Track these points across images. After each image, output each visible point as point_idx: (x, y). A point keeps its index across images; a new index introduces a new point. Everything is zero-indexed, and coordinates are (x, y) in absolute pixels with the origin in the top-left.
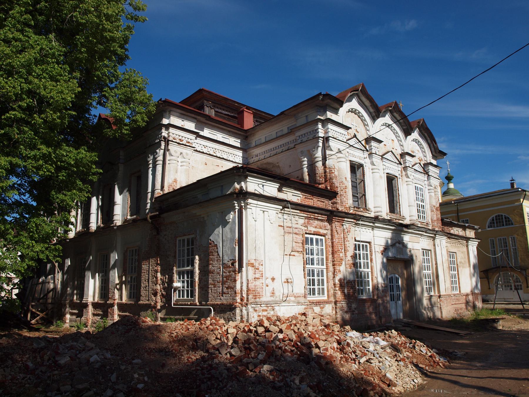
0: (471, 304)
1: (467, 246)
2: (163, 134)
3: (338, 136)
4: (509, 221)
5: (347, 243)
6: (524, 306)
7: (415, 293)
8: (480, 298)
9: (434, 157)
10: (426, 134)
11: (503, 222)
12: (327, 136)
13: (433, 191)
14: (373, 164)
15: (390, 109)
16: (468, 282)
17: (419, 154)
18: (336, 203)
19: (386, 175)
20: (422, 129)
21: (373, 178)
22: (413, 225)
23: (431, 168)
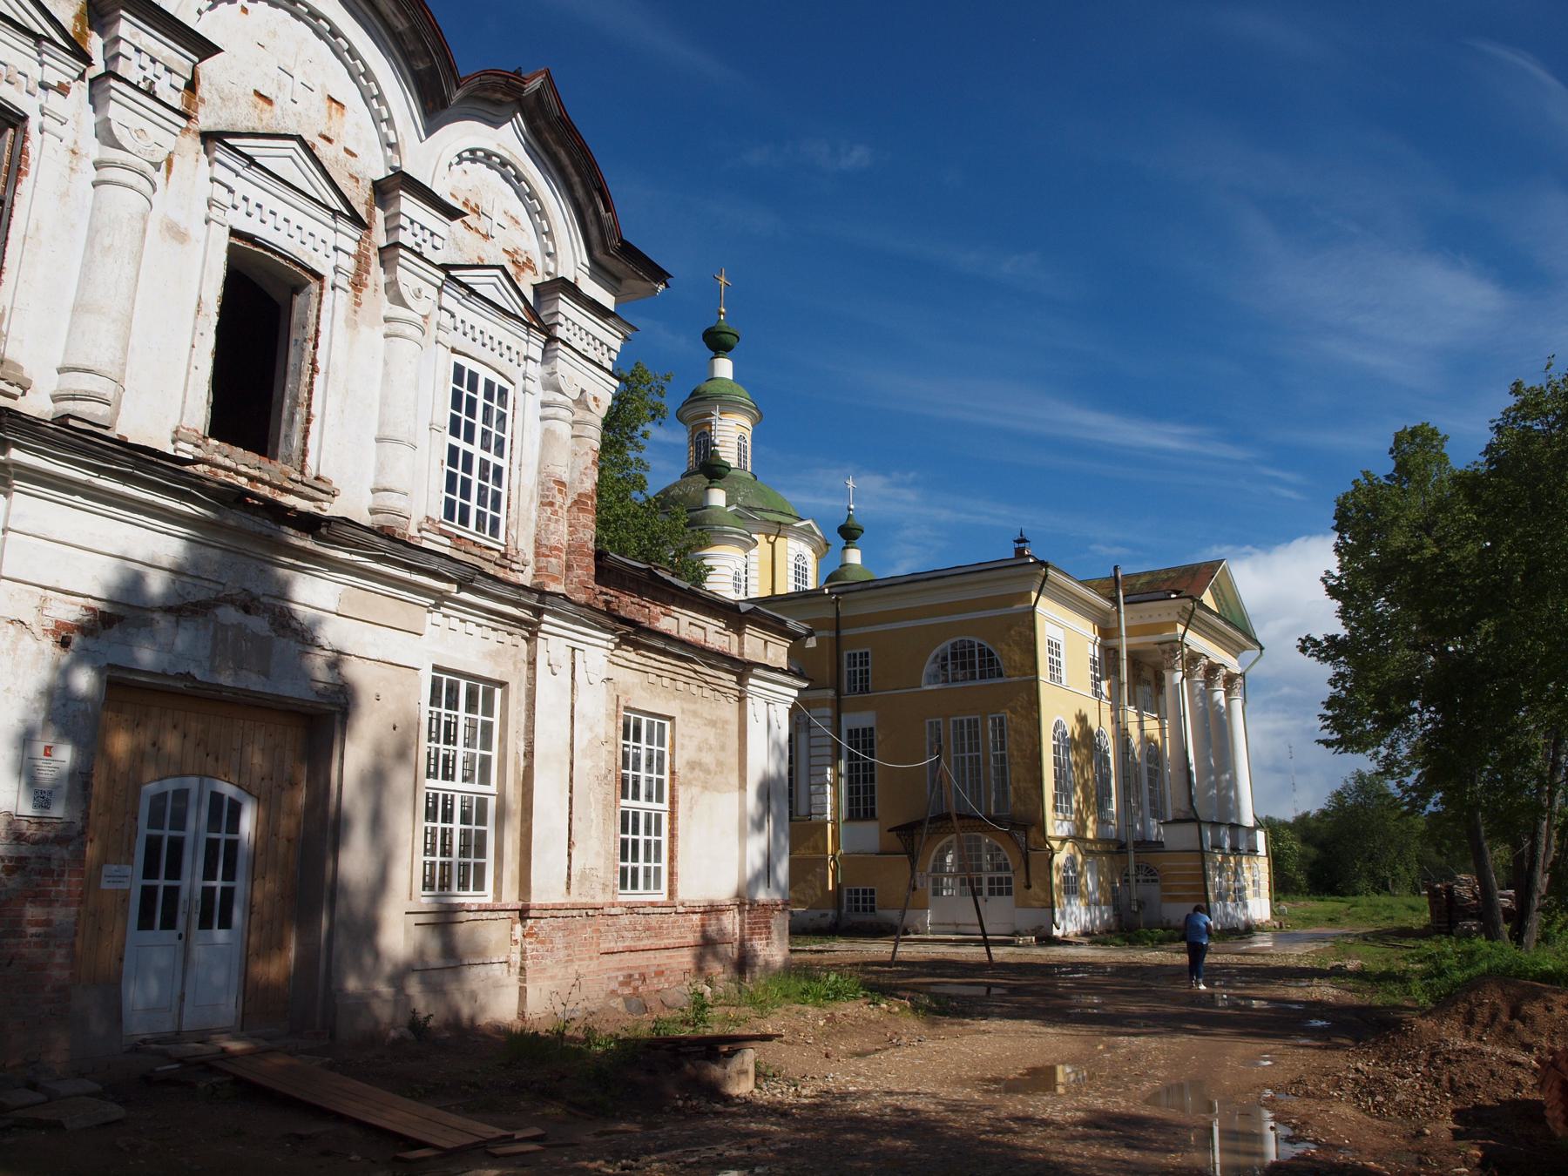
0: (732, 951)
1: (741, 699)
6: (993, 950)
7: (334, 890)
8: (780, 923)
10: (563, 155)
11: (972, 664)
14: (106, 136)
16: (719, 851)
19: (222, 241)
20: (540, 123)
21: (95, 210)
23: (566, 307)
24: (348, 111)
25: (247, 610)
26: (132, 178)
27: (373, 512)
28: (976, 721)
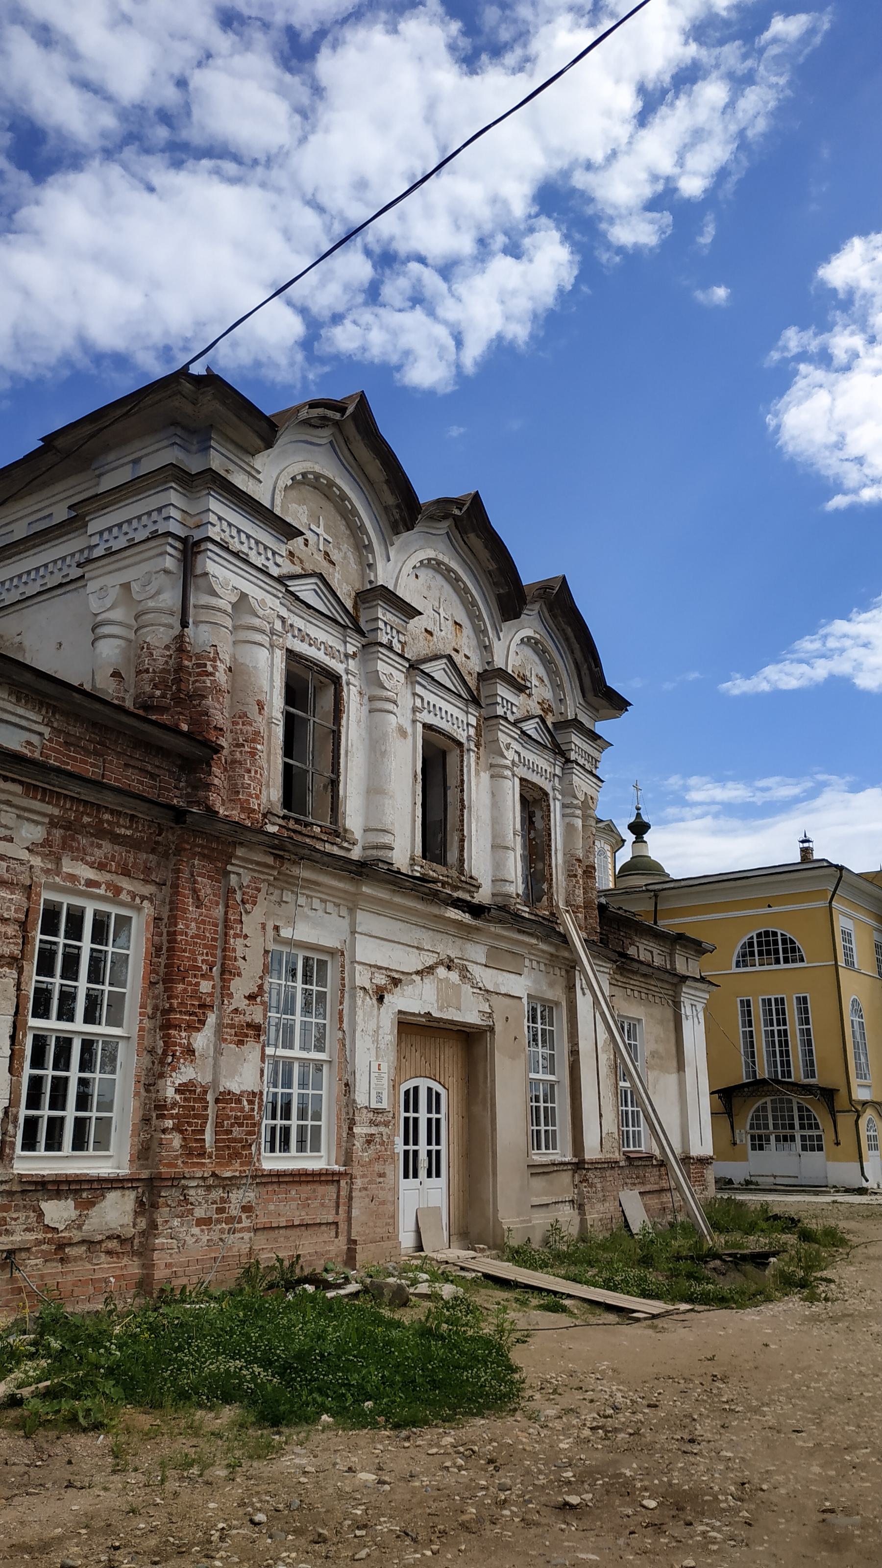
4: (793, 950)
5: (237, 944)
11: (776, 951)
12: (197, 535)
15: (456, 512)
17: (542, 691)
22: (503, 908)
24: (464, 630)
25: (449, 968)
28: (782, 999)
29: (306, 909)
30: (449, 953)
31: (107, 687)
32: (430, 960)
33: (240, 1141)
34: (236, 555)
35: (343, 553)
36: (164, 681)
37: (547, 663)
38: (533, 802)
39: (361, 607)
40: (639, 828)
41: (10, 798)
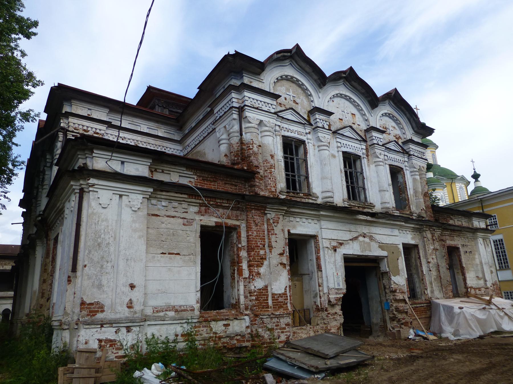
2: (62, 125)
3: (260, 106)
9: (417, 133)
13: (417, 173)
15: (344, 75)
18: (254, 186)
24: (356, 116)
25: (364, 237)
26: (268, 133)
27: (382, 208)
29: (300, 223)
30: (363, 231)
31: (225, 161)
32: (355, 235)
33: (282, 302)
34: (257, 108)
35: (302, 99)
36: (237, 154)
37: (396, 120)
38: (395, 172)
39: (311, 116)
40: (476, 176)
41: (184, 199)
